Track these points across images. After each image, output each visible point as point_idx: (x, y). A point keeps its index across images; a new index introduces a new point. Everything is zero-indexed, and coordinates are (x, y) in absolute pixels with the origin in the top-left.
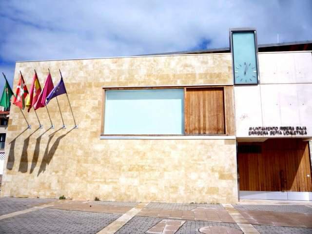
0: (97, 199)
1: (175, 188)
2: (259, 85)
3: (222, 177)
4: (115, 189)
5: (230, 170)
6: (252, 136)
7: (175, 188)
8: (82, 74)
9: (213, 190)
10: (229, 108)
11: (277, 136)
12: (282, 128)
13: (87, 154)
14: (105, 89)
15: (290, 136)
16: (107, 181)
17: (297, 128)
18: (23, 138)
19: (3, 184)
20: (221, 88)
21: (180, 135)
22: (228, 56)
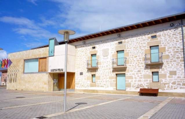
0: (22, 90)
1: (36, 87)
2: (54, 56)
3: (45, 84)
4: (25, 87)
5: (46, 82)
6: (52, 72)
7: (36, 87)
8: (20, 56)
9: (43, 88)
10: (47, 64)
11: (57, 72)
12: (58, 69)
13: (20, 78)
14: (25, 60)
15: (60, 72)
16: (160, 59)
17: (61, 69)
18: (10, 74)
19: (181, 55)
20: (45, 58)
21: (66, 71)
22: (48, 48)
